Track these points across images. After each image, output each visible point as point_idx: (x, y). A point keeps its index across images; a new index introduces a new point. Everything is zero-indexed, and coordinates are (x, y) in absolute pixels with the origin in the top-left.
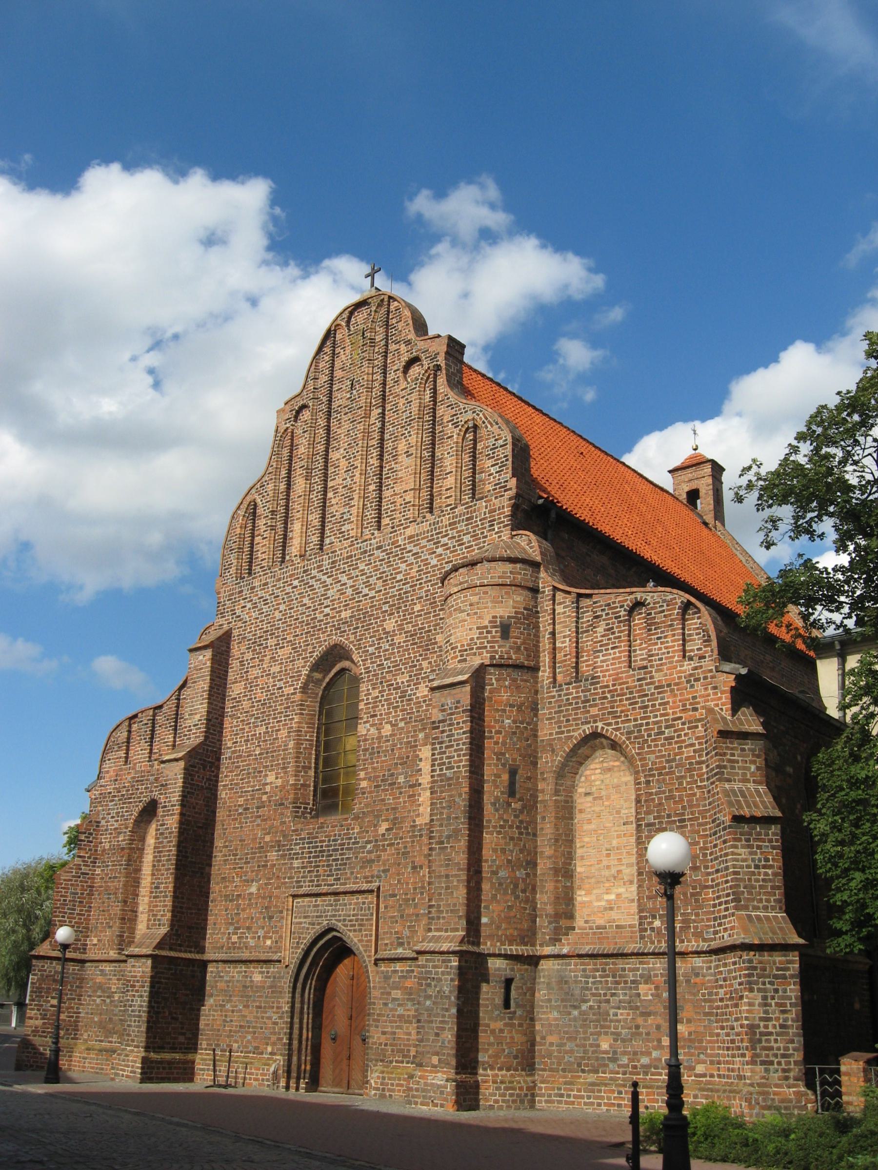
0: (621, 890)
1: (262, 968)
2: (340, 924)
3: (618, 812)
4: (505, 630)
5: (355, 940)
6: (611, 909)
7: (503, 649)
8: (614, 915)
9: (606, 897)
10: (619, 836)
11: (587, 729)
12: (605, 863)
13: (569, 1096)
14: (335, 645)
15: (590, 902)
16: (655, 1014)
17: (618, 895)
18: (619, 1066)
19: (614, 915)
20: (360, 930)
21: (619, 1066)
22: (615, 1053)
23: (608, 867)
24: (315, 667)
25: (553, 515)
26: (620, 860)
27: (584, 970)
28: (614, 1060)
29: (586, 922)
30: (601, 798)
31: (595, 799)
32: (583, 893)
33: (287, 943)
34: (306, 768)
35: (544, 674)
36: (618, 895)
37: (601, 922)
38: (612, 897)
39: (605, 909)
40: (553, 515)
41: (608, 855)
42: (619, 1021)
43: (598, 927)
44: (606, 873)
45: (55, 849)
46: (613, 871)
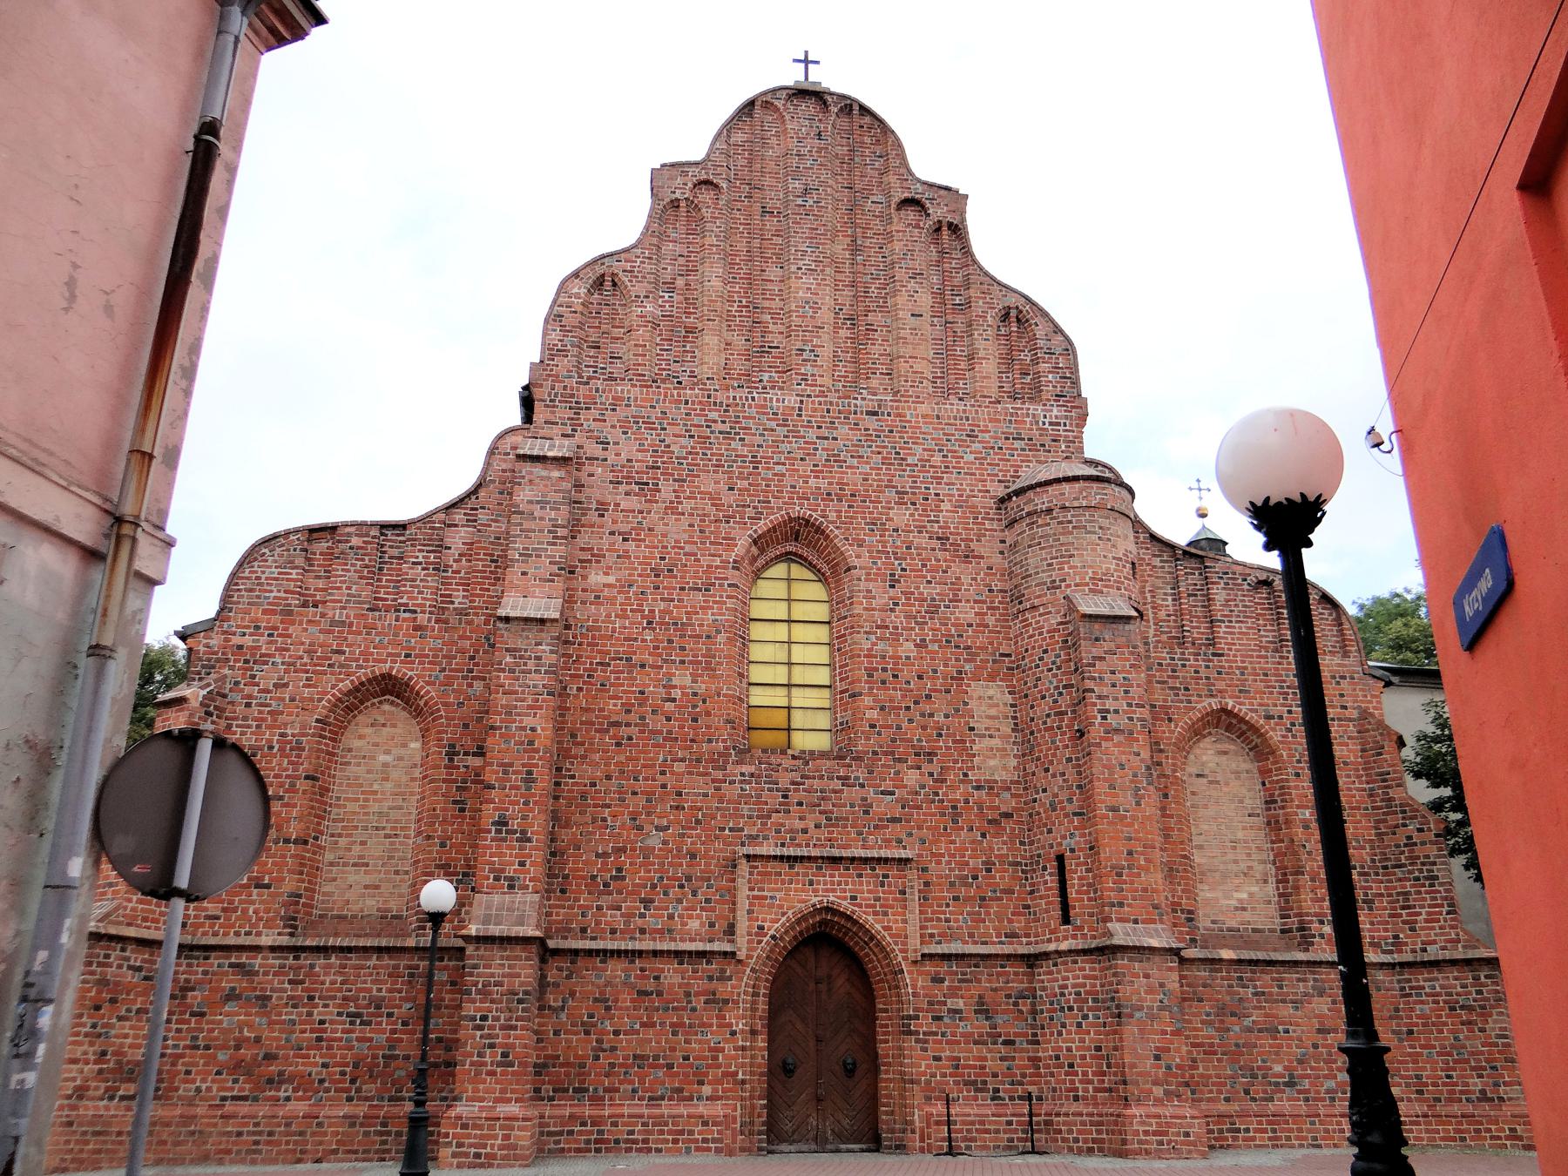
0: (1255, 889)
1: (123, 950)
2: (844, 903)
3: (1241, 802)
5: (878, 927)
6: (1244, 909)
8: (1247, 916)
9: (1236, 895)
10: (1244, 828)
12: (1230, 856)
13: (1247, 1130)
14: (819, 530)
15: (1217, 899)
16: (1335, 1031)
17: (1251, 895)
18: (1299, 1092)
19: (1247, 916)
20: (886, 914)
21: (1299, 1092)
22: (1291, 1076)
23: (1236, 862)
26: (1249, 855)
27: (1241, 978)
28: (1291, 1084)
29: (1214, 922)
30: (1217, 782)
31: (1211, 782)
32: (1206, 887)
36: (1251, 895)
38: (1245, 896)
39: (1237, 909)
41: (1234, 848)
42: (1291, 1039)
43: (1230, 930)
44: (1234, 867)
45: (1098, 442)
46: (1243, 866)
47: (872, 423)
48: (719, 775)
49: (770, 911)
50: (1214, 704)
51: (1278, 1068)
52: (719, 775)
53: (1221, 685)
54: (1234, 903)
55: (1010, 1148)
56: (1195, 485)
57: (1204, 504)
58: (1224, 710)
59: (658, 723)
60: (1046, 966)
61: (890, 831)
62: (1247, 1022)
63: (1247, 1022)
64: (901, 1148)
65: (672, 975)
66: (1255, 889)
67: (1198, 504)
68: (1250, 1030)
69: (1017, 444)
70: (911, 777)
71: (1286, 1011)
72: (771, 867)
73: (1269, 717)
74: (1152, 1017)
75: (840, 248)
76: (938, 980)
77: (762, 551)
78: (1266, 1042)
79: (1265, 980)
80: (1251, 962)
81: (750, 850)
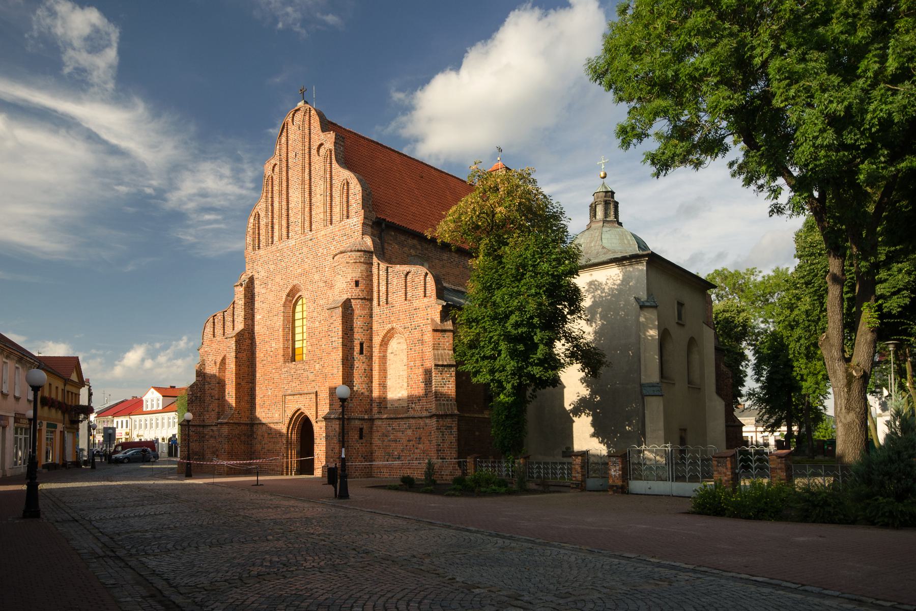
4: (357, 283)
11: (389, 326)
24: (288, 295)
35: (375, 302)
47: (310, 243)
59: (269, 359)
61: (314, 384)
69: (345, 238)
70: (317, 366)
71: (400, 434)
78: (393, 445)
79: (395, 424)
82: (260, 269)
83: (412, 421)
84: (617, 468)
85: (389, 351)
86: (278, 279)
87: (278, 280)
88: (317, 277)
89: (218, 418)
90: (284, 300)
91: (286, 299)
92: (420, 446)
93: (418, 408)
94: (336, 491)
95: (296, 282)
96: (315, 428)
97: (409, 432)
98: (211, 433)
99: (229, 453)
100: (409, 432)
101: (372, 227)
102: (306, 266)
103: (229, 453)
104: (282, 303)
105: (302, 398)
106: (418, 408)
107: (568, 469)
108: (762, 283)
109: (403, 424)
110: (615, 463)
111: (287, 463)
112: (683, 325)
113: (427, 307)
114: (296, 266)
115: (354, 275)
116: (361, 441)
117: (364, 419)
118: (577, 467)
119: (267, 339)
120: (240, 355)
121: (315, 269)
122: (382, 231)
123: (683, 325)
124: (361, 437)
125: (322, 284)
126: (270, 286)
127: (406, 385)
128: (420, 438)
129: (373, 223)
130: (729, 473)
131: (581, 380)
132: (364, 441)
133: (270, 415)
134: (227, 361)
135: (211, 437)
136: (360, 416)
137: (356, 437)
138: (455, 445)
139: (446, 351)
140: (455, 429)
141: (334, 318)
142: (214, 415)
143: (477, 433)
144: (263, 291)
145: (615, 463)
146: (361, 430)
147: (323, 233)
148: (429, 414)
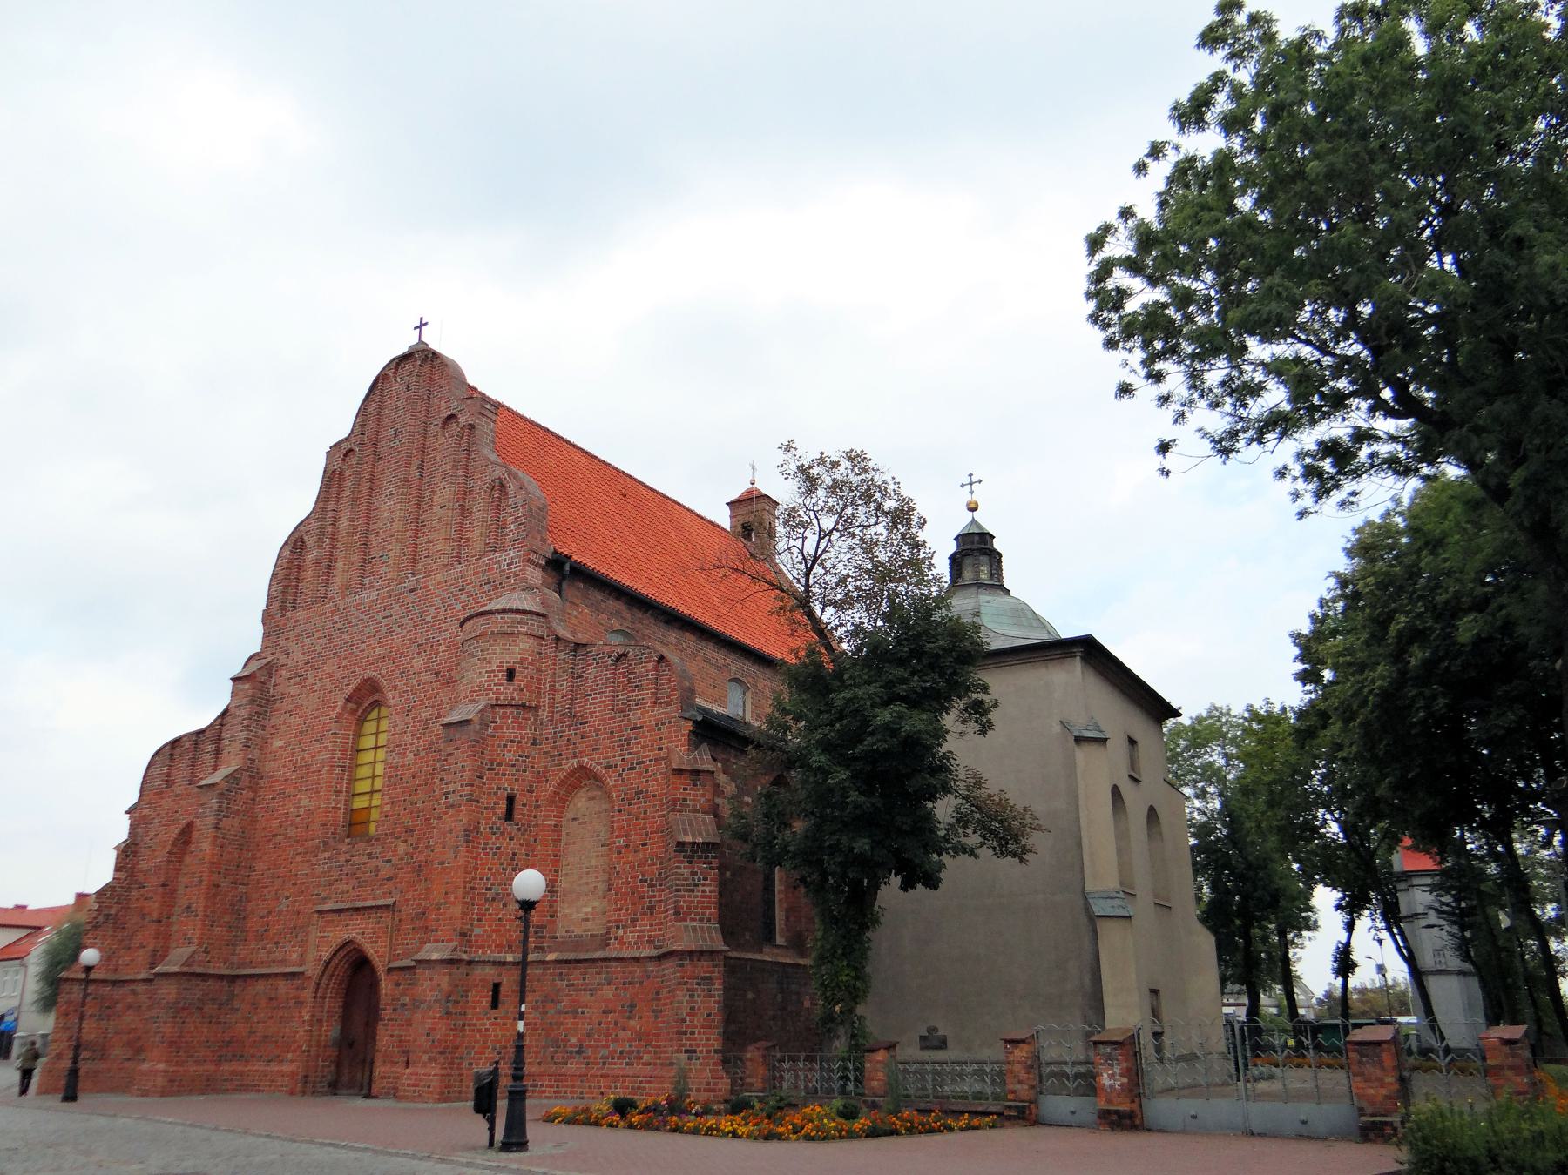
0: (597, 904)
4: (511, 675)
7: (507, 692)
8: (589, 925)
24: (348, 700)
25: (567, 568)
28: (579, 1052)
33: (311, 955)
34: (338, 792)
35: (544, 714)
37: (578, 932)
40: (567, 568)
47: (411, 598)
48: (314, 860)
49: (315, 950)
50: (575, 763)
51: (573, 1040)
52: (314, 860)
53: (581, 747)
54: (582, 916)
55: (292, 1093)
56: (974, 479)
57: (975, 498)
58: (581, 767)
59: (291, 832)
60: (239, 982)
61: (388, 886)
62: (559, 1007)
63: (559, 1007)
64: (395, 1095)
65: (283, 987)
66: (597, 904)
67: (968, 498)
68: (559, 1012)
69: (487, 587)
70: (402, 847)
71: (586, 997)
72: (330, 917)
73: (608, 767)
74: (430, 1008)
75: (414, 472)
76: (398, 984)
77: (359, 705)
79: (575, 975)
80: (567, 962)
81: (320, 908)
82: (292, 646)
83: (616, 968)
84: (1117, 1070)
85: (570, 815)
86: (328, 668)
87: (328, 668)
88: (418, 662)
89: (152, 965)
90: (338, 709)
91: (344, 708)
92: (632, 1023)
93: (630, 937)
94: (492, 1129)
95: (369, 673)
96: (383, 984)
97: (608, 992)
98: (130, 1000)
99: (171, 1043)
100: (608, 992)
101: (544, 569)
102: (397, 640)
103: (171, 1043)
104: (334, 714)
105: (357, 920)
106: (630, 937)
107: (856, 1069)
108: (1192, 728)
109: (595, 976)
110: (1109, 1057)
111: (1246, 1066)
112: (1137, 781)
113: (659, 724)
114: (374, 642)
115: (507, 657)
116: (494, 1013)
117: (504, 963)
118: (1017, 1067)
119: (291, 791)
120: (224, 823)
121: (415, 648)
122: (563, 577)
123: (1137, 781)
124: (495, 1004)
125: (427, 678)
126: (310, 680)
127: (602, 887)
128: (633, 1006)
129: (549, 562)
130: (1389, 1079)
131: (936, 888)
132: (500, 1011)
133: (278, 956)
134: (195, 835)
135: (130, 1007)
136: (497, 956)
137: (486, 1003)
138: (717, 1021)
139: (700, 816)
140: (718, 985)
141: (456, 744)
142: (142, 956)
143: (750, 996)
144: (293, 690)
145: (1109, 1057)
146: (497, 986)
147: (439, 578)
148: (655, 952)
